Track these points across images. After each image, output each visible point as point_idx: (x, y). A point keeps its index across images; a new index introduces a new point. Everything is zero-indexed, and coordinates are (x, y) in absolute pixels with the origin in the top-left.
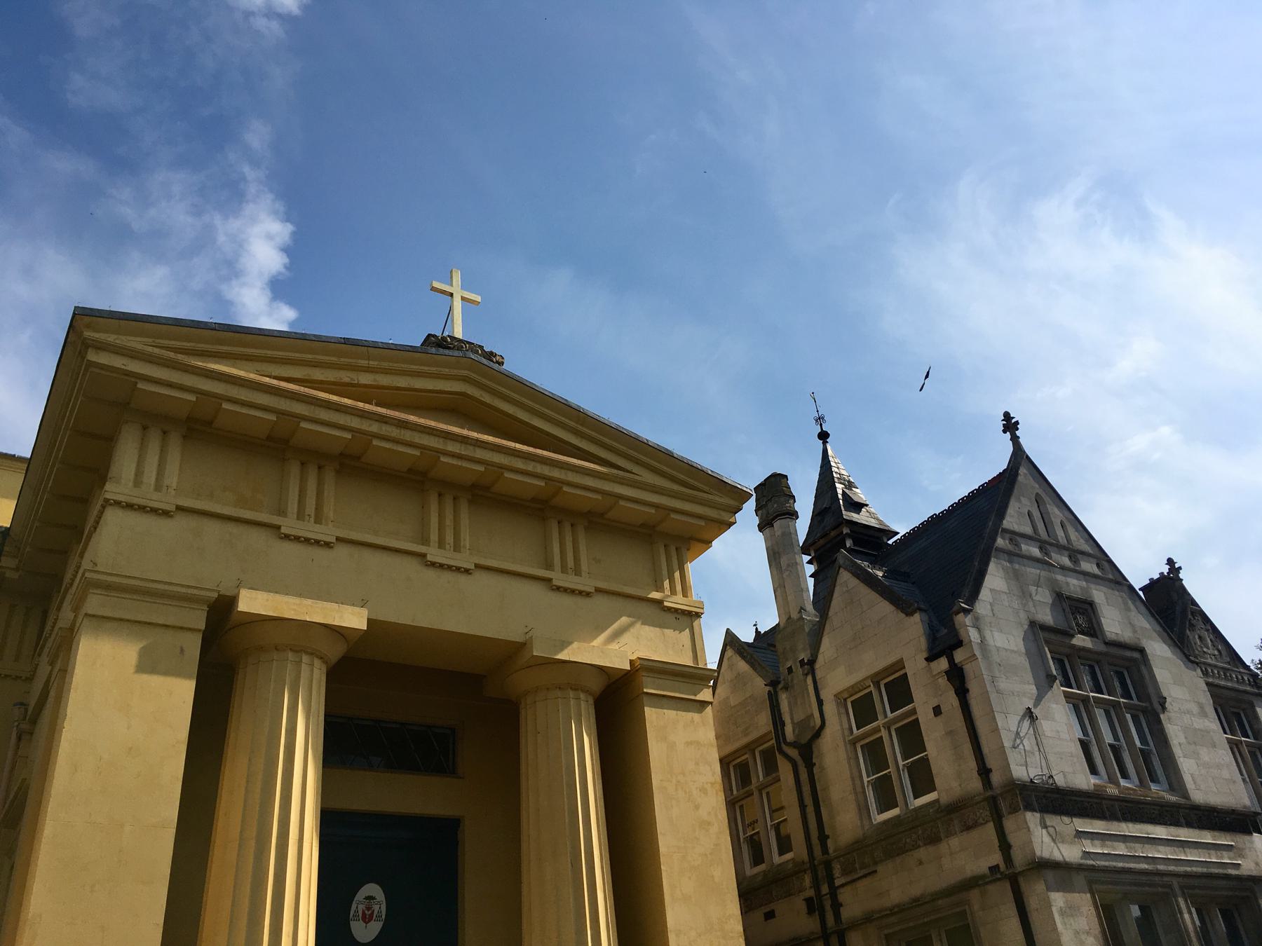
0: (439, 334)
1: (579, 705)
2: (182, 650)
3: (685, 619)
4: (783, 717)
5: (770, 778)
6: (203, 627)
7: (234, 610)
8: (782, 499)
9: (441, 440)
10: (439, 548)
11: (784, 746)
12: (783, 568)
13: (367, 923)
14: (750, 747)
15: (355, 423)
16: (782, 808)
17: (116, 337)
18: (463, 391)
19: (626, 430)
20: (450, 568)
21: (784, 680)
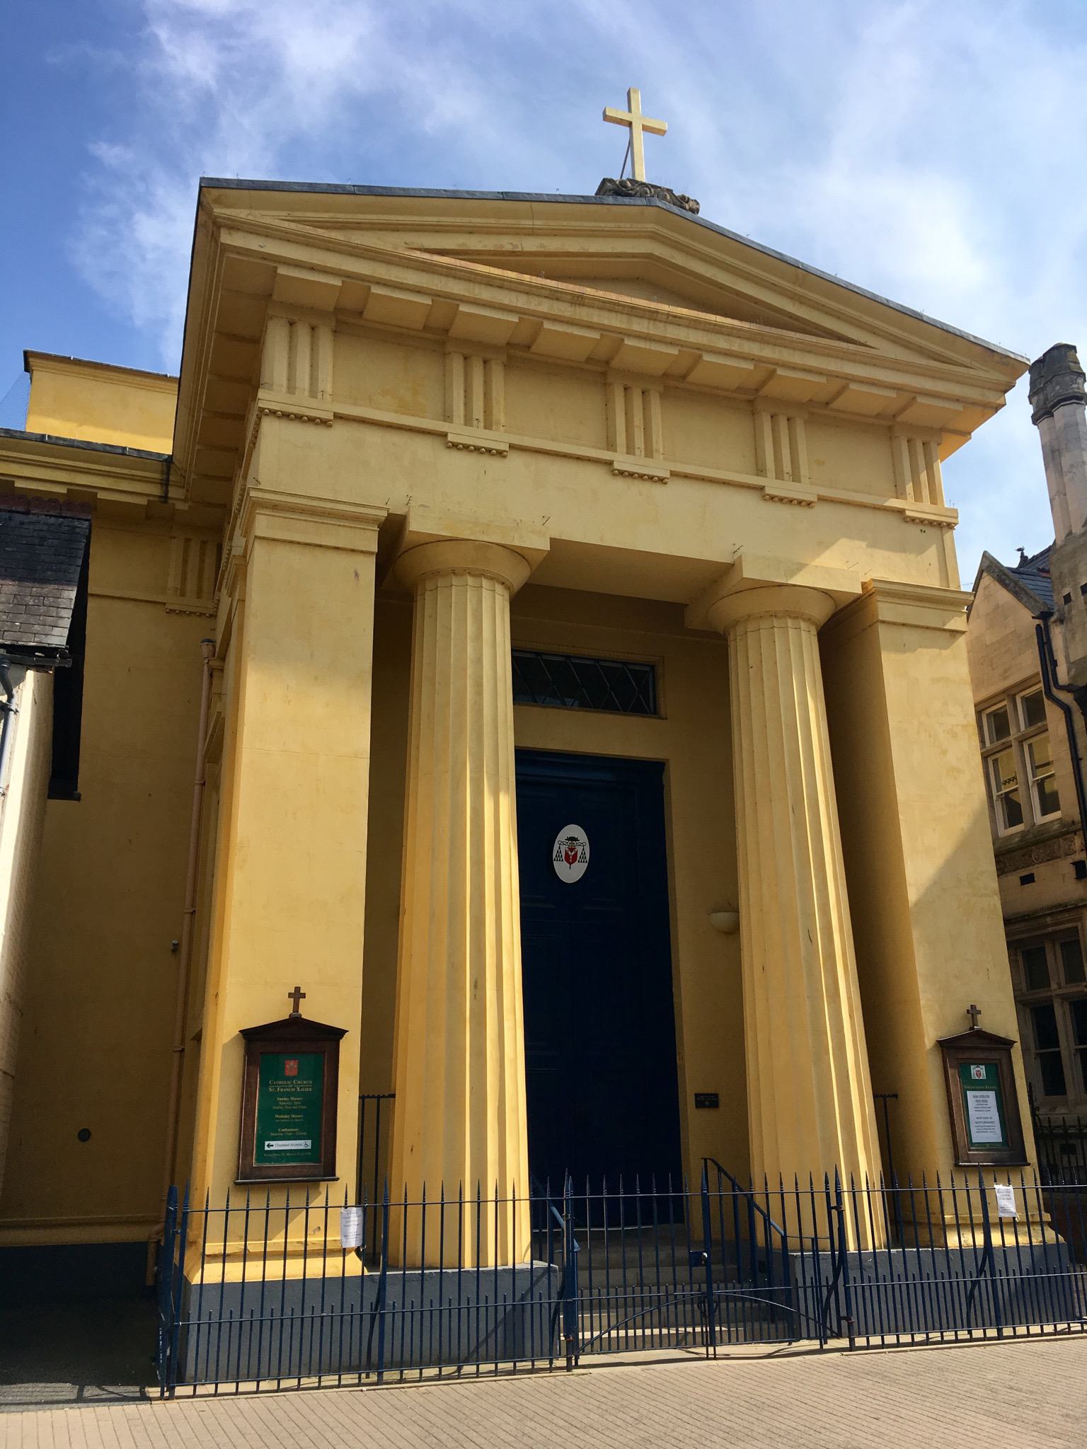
0: (617, 178)
1: (800, 637)
2: (357, 575)
3: (931, 532)
4: (1055, 654)
5: (1033, 728)
6: (374, 548)
7: (405, 530)
8: (1067, 378)
9: (625, 317)
10: (627, 453)
11: (1054, 691)
12: (1065, 469)
13: (570, 864)
14: (1009, 693)
15: (520, 301)
16: (1048, 764)
17: (248, 211)
18: (649, 251)
19: (858, 288)
20: (641, 476)
21: (1058, 611)
